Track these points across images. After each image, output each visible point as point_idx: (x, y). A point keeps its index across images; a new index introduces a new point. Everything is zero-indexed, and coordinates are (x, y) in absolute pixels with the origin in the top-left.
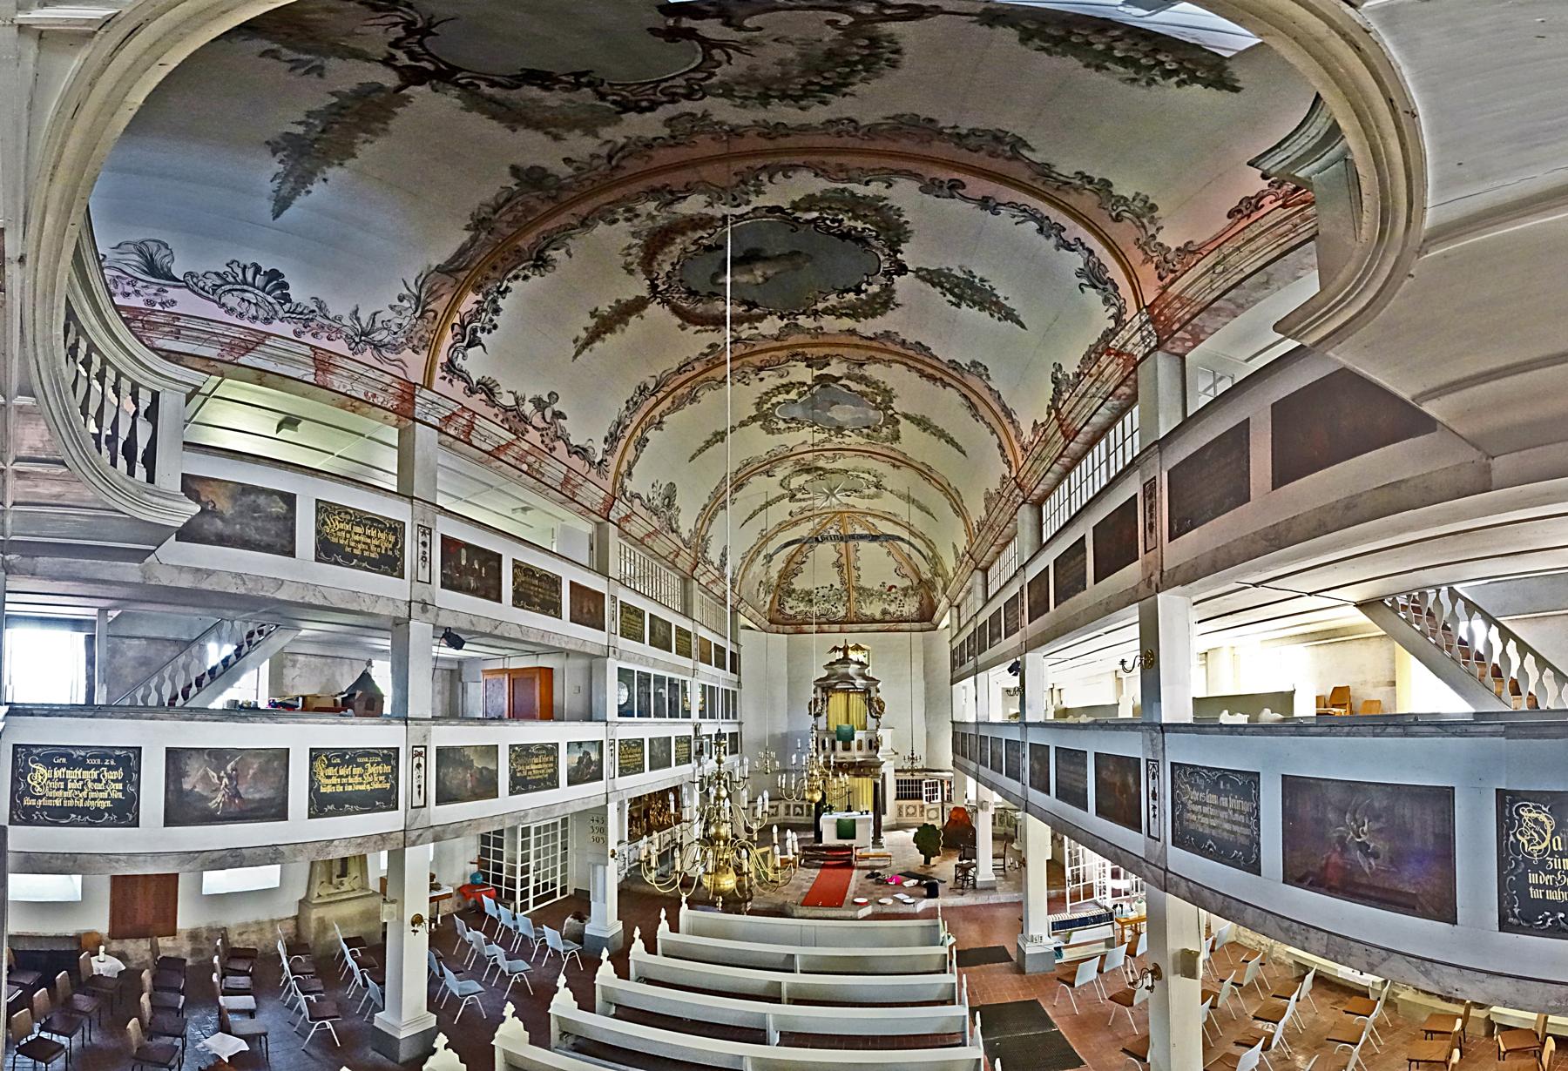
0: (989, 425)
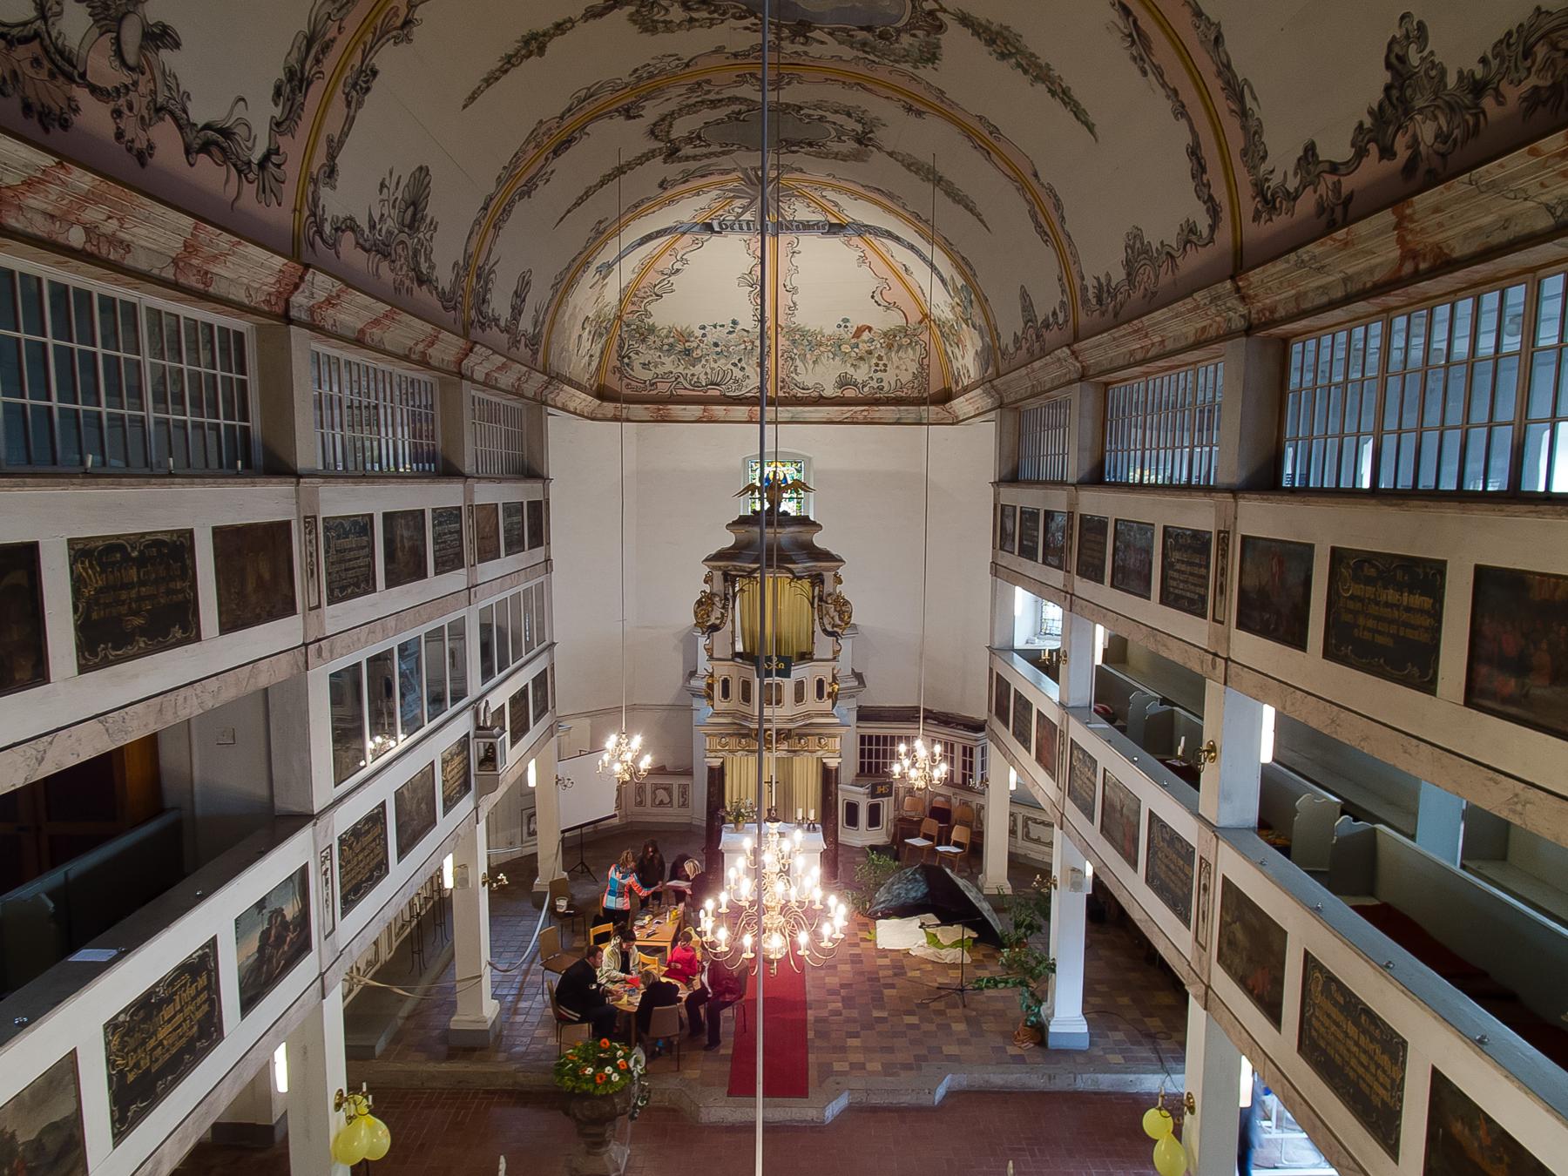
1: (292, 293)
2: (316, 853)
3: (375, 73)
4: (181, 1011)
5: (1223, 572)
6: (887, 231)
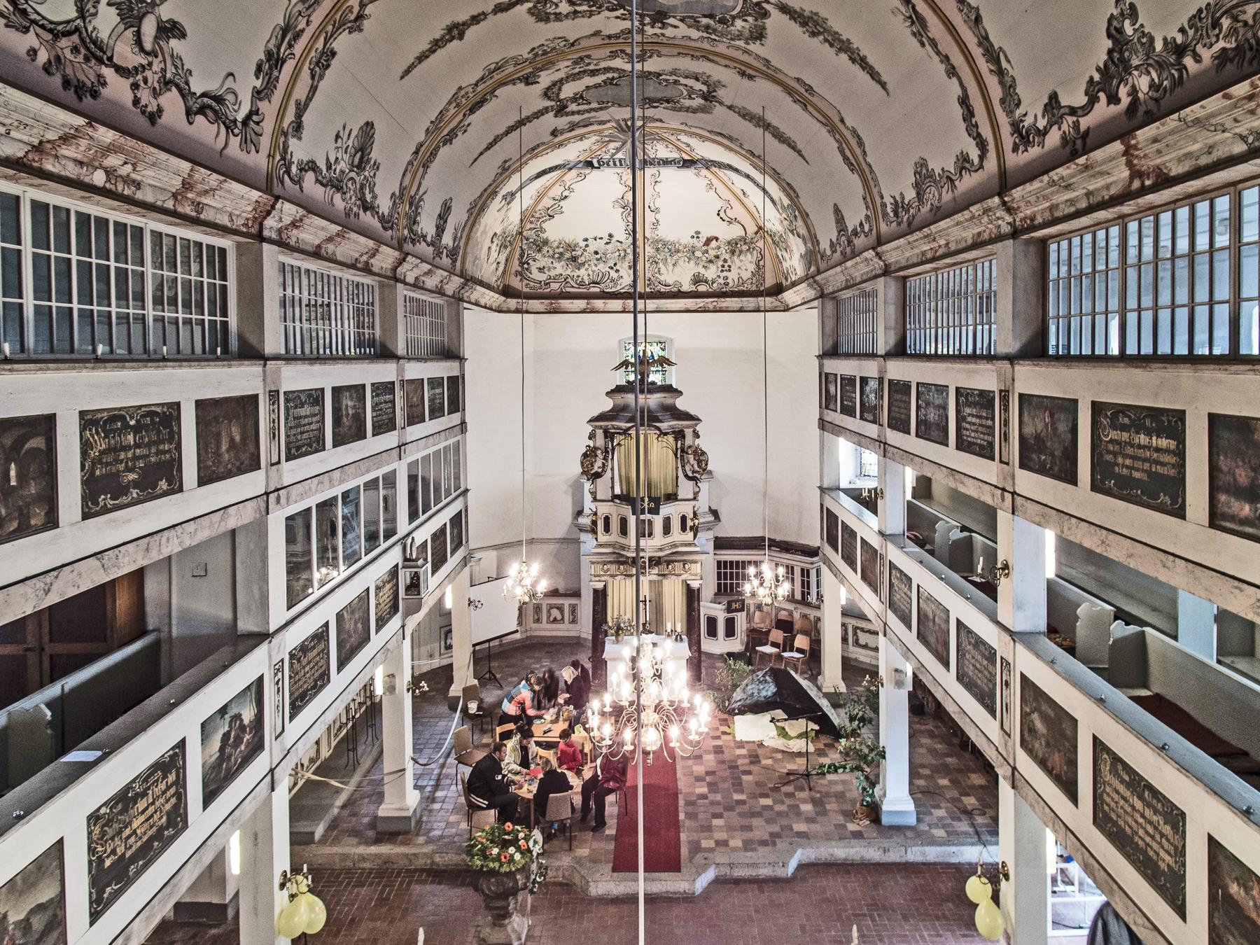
0: (946, 59)
1: (265, 218)
3: (333, 54)
4: (153, 803)
5: (1006, 423)
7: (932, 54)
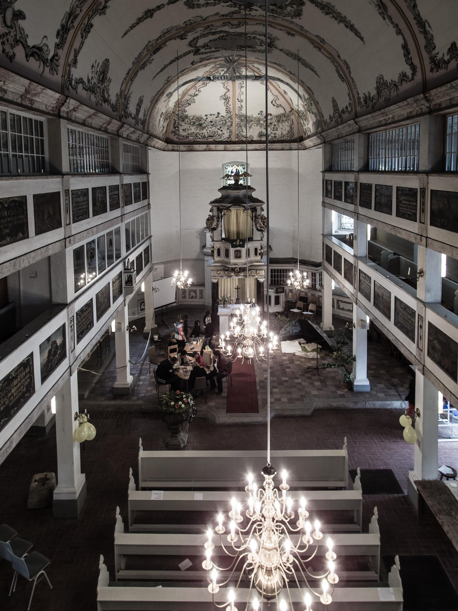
0: (396, 26)
1: (61, 107)
2: (68, 319)
3: (92, 26)
4: (20, 382)
5: (423, 204)
6: (278, 78)
7: (389, 23)
